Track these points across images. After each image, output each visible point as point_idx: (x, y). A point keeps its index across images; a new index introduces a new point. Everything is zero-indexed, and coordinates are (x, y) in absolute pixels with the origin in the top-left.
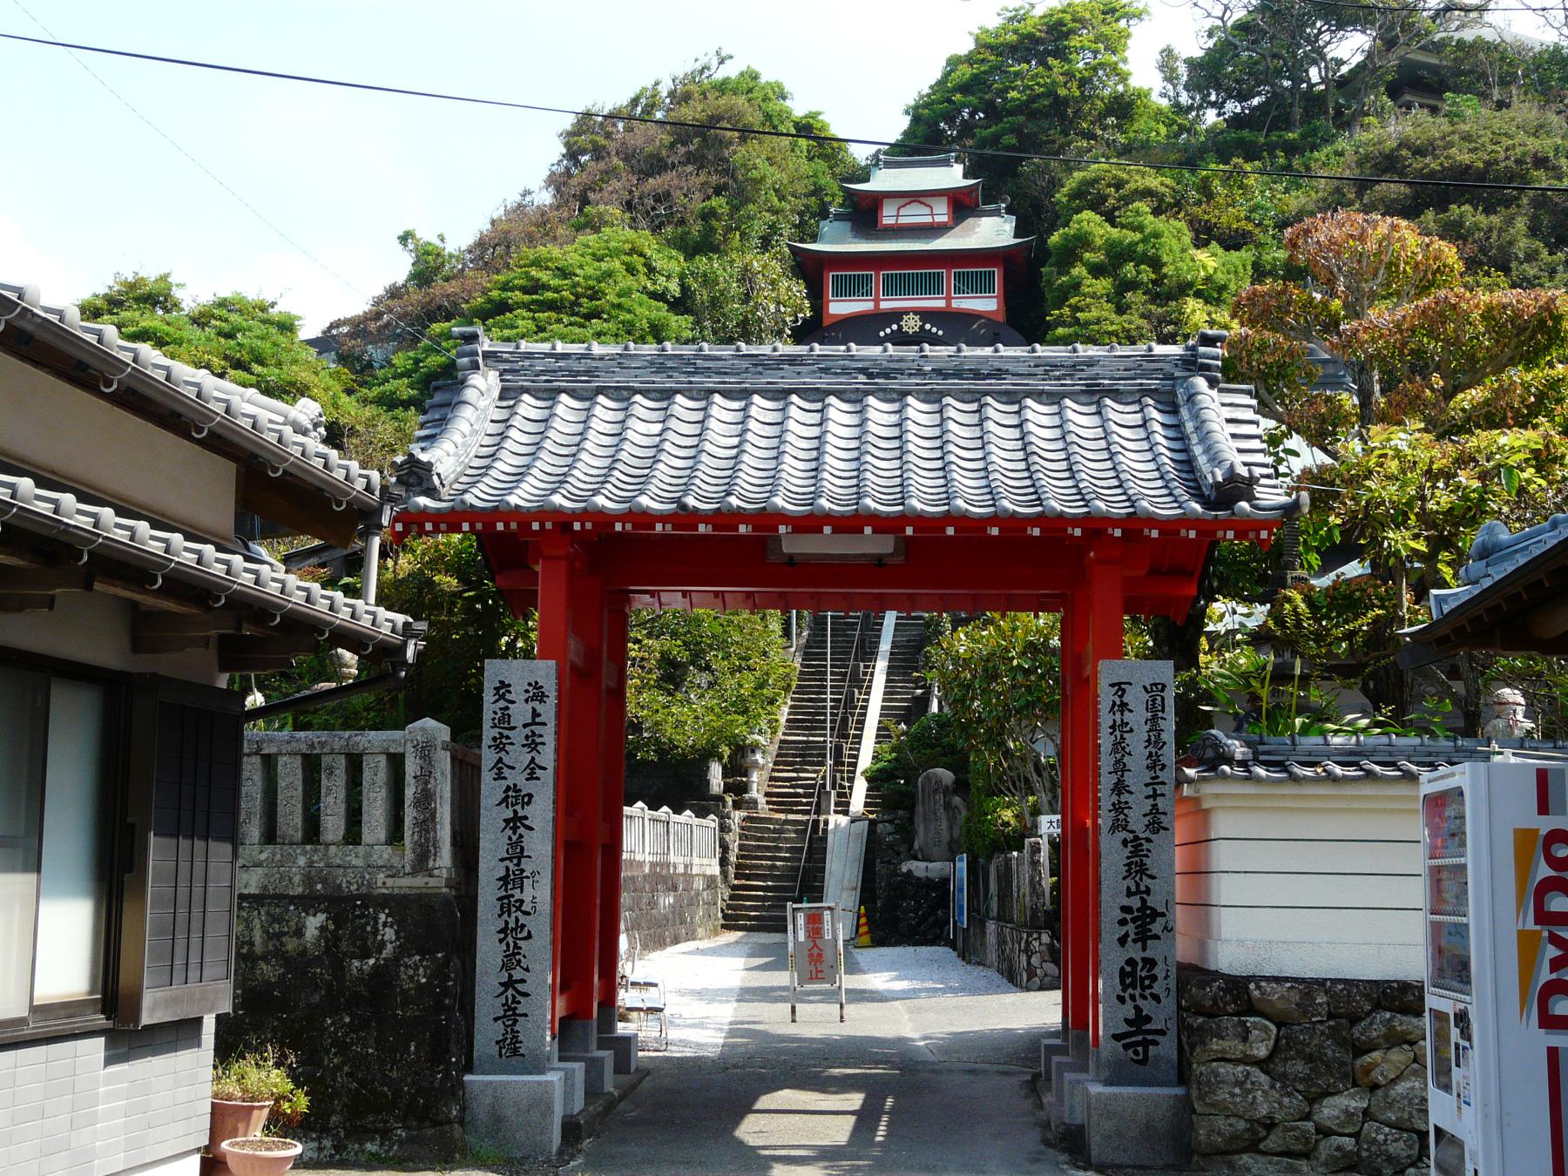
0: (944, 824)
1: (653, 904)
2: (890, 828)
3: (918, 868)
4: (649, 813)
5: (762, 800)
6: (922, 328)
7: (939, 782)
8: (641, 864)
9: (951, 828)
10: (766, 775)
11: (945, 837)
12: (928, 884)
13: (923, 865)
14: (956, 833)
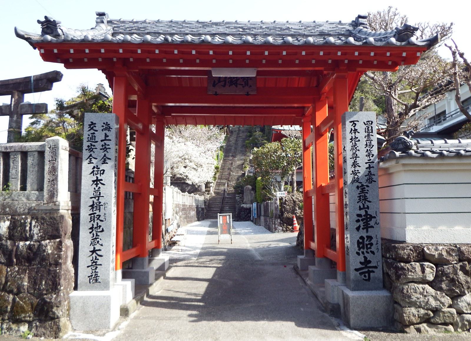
0: (250, 197)
1: (190, 213)
2: (238, 198)
3: (244, 206)
4: (188, 195)
5: (213, 193)
6: (19, 327)
7: (249, 188)
8: (187, 205)
9: (251, 198)
10: (214, 188)
11: (250, 199)
12: (246, 209)
13: (245, 205)
14: (252, 198)
